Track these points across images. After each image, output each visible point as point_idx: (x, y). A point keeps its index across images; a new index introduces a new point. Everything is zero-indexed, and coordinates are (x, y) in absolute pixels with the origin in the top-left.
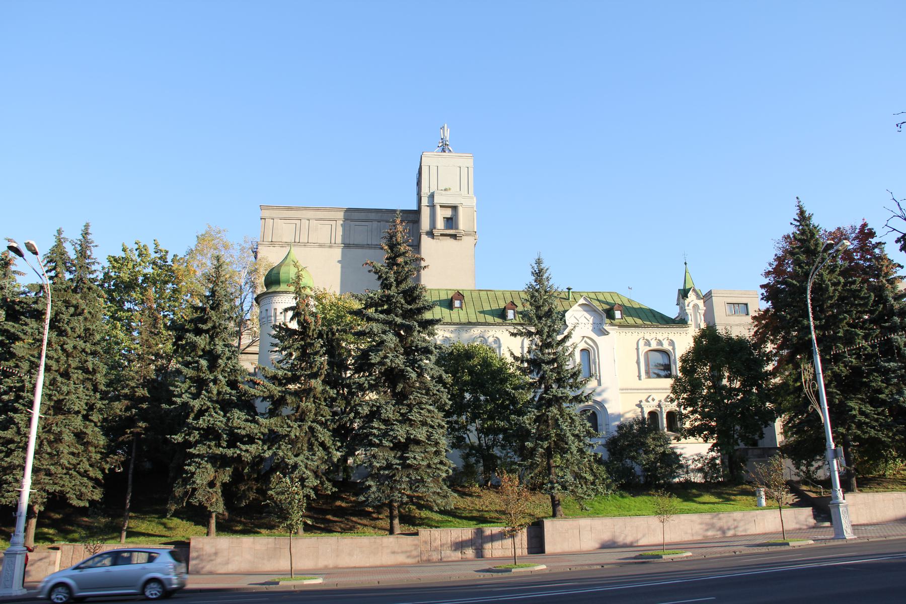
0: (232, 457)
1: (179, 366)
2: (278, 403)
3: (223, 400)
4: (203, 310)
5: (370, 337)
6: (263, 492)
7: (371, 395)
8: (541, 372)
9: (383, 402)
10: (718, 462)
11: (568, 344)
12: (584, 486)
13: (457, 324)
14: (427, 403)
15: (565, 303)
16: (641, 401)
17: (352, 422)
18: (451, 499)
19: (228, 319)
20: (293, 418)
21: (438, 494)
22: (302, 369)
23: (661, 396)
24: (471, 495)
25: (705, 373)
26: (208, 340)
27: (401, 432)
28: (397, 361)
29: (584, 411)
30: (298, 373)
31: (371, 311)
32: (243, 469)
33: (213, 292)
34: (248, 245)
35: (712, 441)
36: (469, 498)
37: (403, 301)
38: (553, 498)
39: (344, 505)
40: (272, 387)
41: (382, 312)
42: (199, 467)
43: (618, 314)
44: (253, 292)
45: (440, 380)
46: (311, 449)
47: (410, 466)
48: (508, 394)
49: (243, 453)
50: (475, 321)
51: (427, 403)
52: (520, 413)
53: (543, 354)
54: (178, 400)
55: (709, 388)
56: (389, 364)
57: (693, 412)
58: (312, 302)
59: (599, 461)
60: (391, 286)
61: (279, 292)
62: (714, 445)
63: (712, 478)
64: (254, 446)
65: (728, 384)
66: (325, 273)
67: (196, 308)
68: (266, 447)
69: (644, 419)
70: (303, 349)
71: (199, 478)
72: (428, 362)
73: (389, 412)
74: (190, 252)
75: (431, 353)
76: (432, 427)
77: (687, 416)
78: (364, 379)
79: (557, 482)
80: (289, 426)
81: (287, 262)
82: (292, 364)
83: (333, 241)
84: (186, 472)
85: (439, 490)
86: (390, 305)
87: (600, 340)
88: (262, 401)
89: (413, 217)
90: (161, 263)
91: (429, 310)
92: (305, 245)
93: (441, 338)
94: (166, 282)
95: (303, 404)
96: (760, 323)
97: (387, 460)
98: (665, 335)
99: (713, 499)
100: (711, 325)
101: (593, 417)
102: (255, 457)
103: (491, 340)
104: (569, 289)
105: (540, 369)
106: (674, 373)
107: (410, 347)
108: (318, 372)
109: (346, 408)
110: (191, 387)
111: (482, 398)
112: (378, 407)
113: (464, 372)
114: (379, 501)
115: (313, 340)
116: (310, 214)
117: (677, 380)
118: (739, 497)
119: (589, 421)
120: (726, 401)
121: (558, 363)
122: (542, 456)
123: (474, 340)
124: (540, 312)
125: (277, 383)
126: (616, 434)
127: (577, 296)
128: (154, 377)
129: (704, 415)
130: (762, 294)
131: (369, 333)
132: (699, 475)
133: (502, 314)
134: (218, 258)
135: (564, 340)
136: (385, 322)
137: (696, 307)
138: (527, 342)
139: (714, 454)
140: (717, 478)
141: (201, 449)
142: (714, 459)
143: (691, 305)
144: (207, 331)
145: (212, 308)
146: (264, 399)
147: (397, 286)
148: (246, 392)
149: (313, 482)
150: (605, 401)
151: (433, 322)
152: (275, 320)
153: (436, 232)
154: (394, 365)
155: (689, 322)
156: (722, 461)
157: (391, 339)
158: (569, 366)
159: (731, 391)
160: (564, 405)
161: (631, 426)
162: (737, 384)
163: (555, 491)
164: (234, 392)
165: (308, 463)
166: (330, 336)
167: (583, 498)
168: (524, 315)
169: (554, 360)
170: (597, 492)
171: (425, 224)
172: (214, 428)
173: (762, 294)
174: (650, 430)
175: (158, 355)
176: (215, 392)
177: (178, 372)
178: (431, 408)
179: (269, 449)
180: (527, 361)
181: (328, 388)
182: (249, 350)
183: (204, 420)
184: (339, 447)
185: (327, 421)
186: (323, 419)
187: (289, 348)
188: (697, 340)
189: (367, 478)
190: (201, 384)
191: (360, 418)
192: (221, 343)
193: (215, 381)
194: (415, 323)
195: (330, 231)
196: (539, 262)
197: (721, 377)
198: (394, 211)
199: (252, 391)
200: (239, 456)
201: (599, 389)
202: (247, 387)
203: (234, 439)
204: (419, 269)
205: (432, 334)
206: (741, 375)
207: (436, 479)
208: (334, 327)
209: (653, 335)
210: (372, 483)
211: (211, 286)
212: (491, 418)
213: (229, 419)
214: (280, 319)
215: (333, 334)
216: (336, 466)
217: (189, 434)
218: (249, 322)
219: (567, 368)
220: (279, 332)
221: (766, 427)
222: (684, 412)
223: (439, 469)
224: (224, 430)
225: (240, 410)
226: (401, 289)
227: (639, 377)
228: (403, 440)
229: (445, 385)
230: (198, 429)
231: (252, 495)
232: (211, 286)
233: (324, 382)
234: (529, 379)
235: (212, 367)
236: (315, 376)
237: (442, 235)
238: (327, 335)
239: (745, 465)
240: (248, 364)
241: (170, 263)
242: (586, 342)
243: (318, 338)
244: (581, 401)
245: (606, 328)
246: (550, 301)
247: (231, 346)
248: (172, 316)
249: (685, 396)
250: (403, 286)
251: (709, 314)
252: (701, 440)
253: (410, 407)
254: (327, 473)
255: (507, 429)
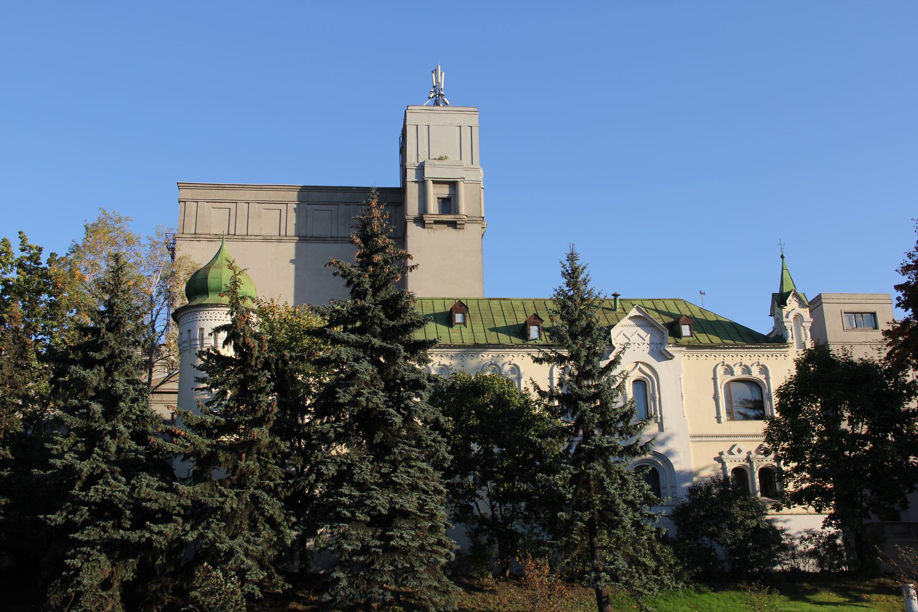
0: (139, 542)
1: (58, 412)
2: (205, 463)
3: (126, 460)
4: (95, 331)
5: (337, 367)
6: (183, 593)
7: (339, 448)
8: (578, 413)
9: (356, 458)
10: (839, 541)
11: (615, 372)
12: (643, 577)
13: (459, 347)
14: (417, 459)
15: (611, 315)
16: (721, 453)
17: (312, 487)
18: (453, 596)
19: (134, 344)
20: (229, 483)
21: (436, 588)
22: (241, 413)
23: (750, 446)
24: (481, 590)
25: (814, 412)
26: (103, 375)
27: (381, 500)
28: (375, 399)
29: (639, 468)
30: (235, 420)
31: (338, 329)
32: (154, 560)
33: (110, 306)
34: (162, 240)
35: (829, 511)
36: (480, 595)
37: (382, 315)
38: (599, 593)
39: (300, 607)
40: (197, 439)
41: (354, 331)
42: (87, 560)
43: (685, 330)
44: (170, 305)
45: (436, 425)
46: (253, 527)
47: (395, 549)
48: (532, 444)
49: (155, 537)
50: (483, 342)
51: (417, 459)
52: (551, 470)
53: (580, 387)
54: (58, 462)
55: (820, 434)
56: (364, 404)
57: (797, 470)
58: (254, 318)
59: (664, 540)
60: (365, 294)
61: (207, 306)
62: (831, 517)
63: (831, 567)
64: (171, 525)
65: (849, 428)
66: (271, 276)
67: (83, 329)
68: (188, 527)
69: (726, 478)
70: (243, 384)
71: (87, 577)
72: (418, 400)
73: (365, 472)
74: (76, 249)
75: (423, 387)
76: (426, 492)
77: (789, 475)
78: (328, 425)
79: (605, 570)
80: (222, 495)
81: (218, 262)
82: (226, 406)
83: (283, 233)
84: (68, 568)
85: (436, 584)
86: (364, 321)
87: (662, 367)
88: (183, 460)
89: (394, 198)
90: (30, 265)
91: (419, 327)
92: (244, 238)
93: (436, 366)
94: (39, 292)
95: (242, 464)
96: (895, 341)
97: (362, 540)
98: (755, 359)
99: (834, 598)
100: (821, 343)
101: (656, 473)
102: (173, 541)
103: (507, 368)
104: (615, 295)
105: (576, 408)
106: (768, 413)
107: (394, 380)
108: (263, 417)
109: (303, 467)
110: (77, 442)
111: (496, 450)
112: (349, 466)
113: (470, 414)
114: (352, 600)
115: (259, 369)
116: (249, 195)
117: (773, 422)
118: (875, 597)
119: (648, 481)
120: (847, 453)
121: (601, 400)
122: (582, 532)
123: (483, 368)
124: (576, 327)
125: (205, 434)
126: (686, 500)
127: (627, 305)
128: (20, 429)
129: (815, 474)
130: (898, 299)
131: (335, 360)
132: (812, 561)
133: (521, 332)
134: (117, 258)
135: (610, 367)
136: (357, 345)
137: (798, 318)
138: (557, 371)
139: (832, 530)
140: (839, 566)
141: (91, 533)
142: (832, 537)
143: (791, 316)
144: (102, 362)
145: (109, 329)
146: (186, 457)
147: (374, 295)
148: (160, 448)
149: (257, 574)
150: (670, 453)
151: (426, 344)
152: (202, 345)
153: (427, 219)
154: (371, 405)
155: (789, 340)
156: (844, 539)
157: (365, 368)
158: (618, 403)
159: (854, 440)
160: (612, 459)
161: (709, 488)
162: (863, 429)
163: (601, 584)
164: (141, 448)
165: (248, 548)
166: (280, 365)
167: (641, 594)
168: (553, 332)
169: (596, 396)
170: (662, 586)
171: (412, 207)
172: (112, 502)
173: (898, 299)
174: (736, 495)
175: (26, 398)
176: (113, 449)
177: (58, 421)
178: (424, 465)
179: (193, 529)
180: (558, 397)
181: (277, 440)
182: (165, 387)
183: (97, 490)
184: (295, 524)
185: (276, 486)
186: (272, 484)
187: (222, 383)
188: (801, 366)
189: (333, 567)
190: (92, 438)
191: (323, 482)
192: (122, 379)
193: (114, 434)
194: (400, 347)
195: (278, 218)
196: (572, 258)
197: (840, 418)
198: (367, 190)
199: (169, 446)
200: (149, 540)
201: (661, 437)
202: (160, 441)
203: (143, 516)
204: (404, 270)
205: (424, 361)
206: (869, 415)
207: (431, 567)
208: (286, 353)
209: (737, 360)
210: (341, 575)
211: (107, 297)
212: (509, 478)
213: (133, 488)
214: (209, 342)
215: (285, 363)
216: (290, 550)
217: (74, 512)
218: (163, 348)
219: (614, 406)
220: (207, 361)
221: (910, 492)
222: (785, 468)
223: (436, 552)
224: (127, 503)
225: (151, 475)
226: (379, 299)
227: (718, 419)
228: (384, 512)
229: (443, 432)
230: (87, 504)
231: (167, 599)
232: (107, 297)
233: (272, 431)
234: (560, 422)
235: (110, 412)
236: (259, 422)
237: (436, 222)
238: (276, 364)
239: (882, 548)
240: (162, 407)
241: (44, 264)
242: (640, 370)
243: (263, 369)
244: (635, 453)
245: (668, 349)
246: (589, 313)
247: (138, 382)
248: (48, 342)
249: (786, 445)
250: (383, 294)
251: (818, 329)
252: (811, 509)
253: (395, 464)
254: (276, 561)
255: (532, 494)
